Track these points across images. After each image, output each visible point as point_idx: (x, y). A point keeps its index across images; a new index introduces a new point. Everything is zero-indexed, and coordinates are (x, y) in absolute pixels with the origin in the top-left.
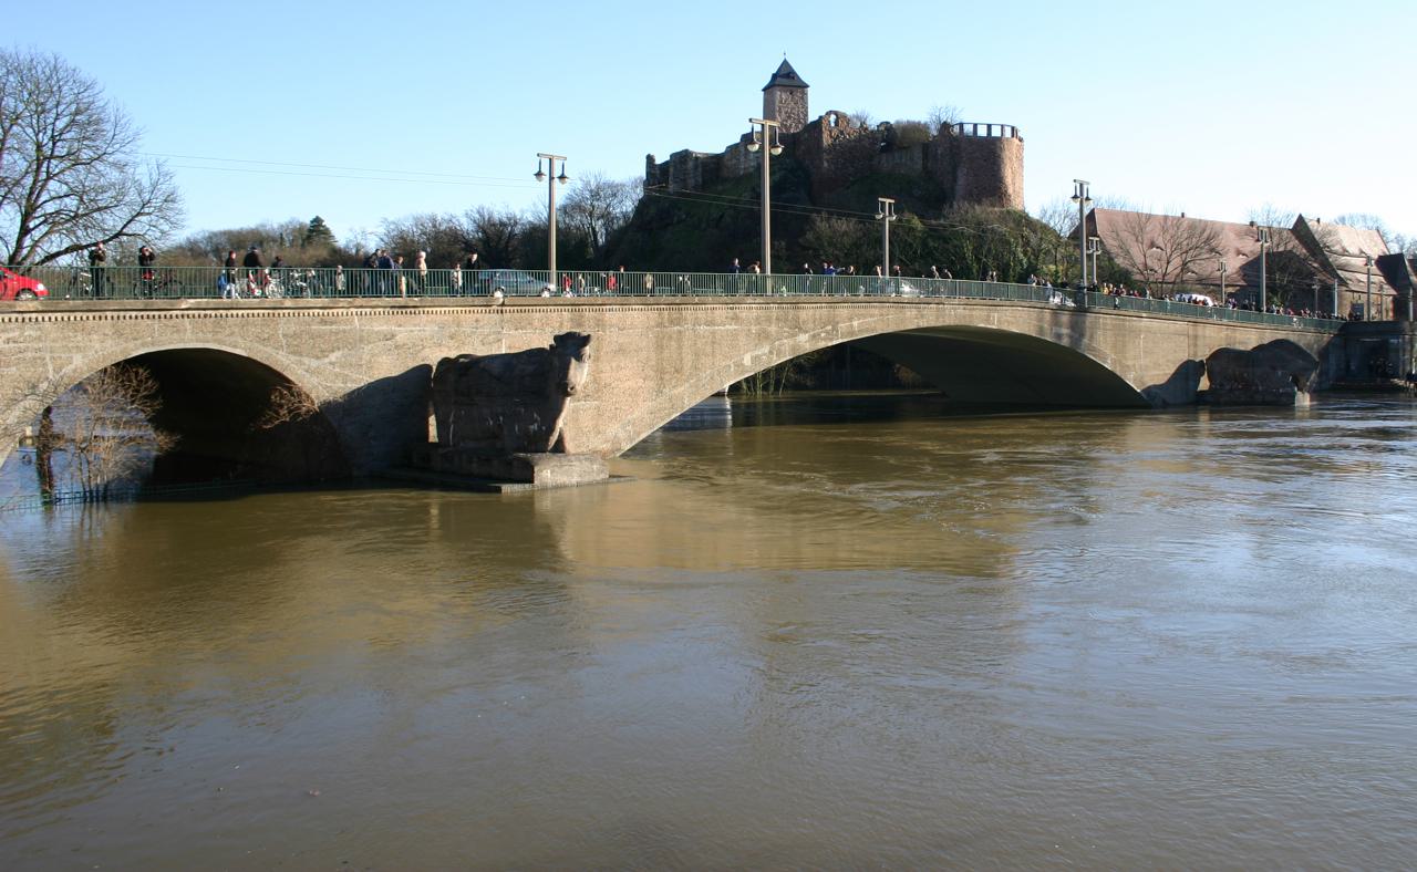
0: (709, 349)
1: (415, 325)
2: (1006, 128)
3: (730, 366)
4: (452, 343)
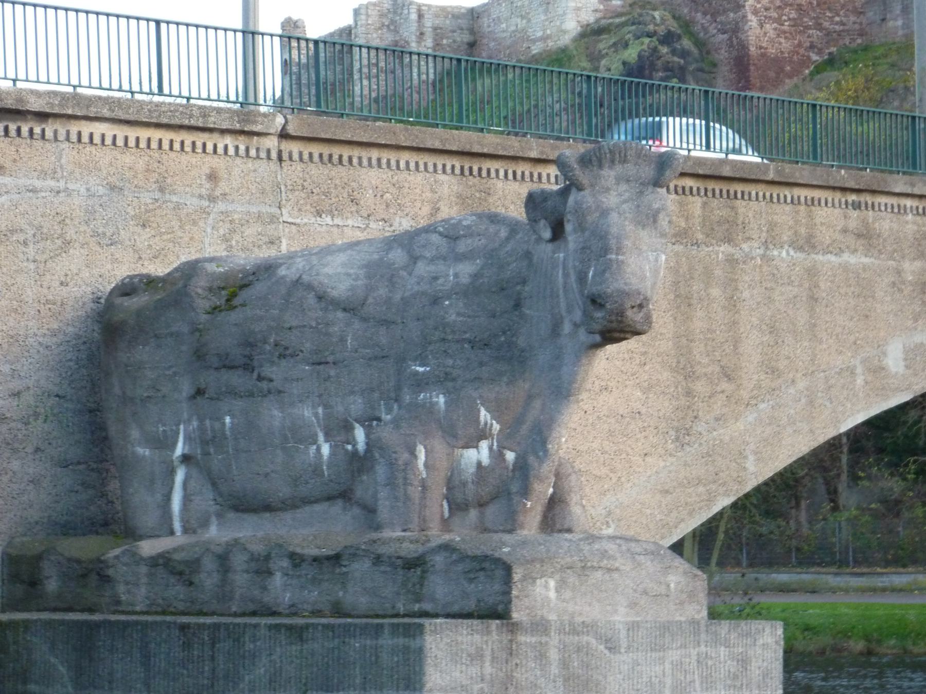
0: (802, 318)
1: (43, 175)
2: (179, 149)
3: (852, 372)
4: (143, 237)
